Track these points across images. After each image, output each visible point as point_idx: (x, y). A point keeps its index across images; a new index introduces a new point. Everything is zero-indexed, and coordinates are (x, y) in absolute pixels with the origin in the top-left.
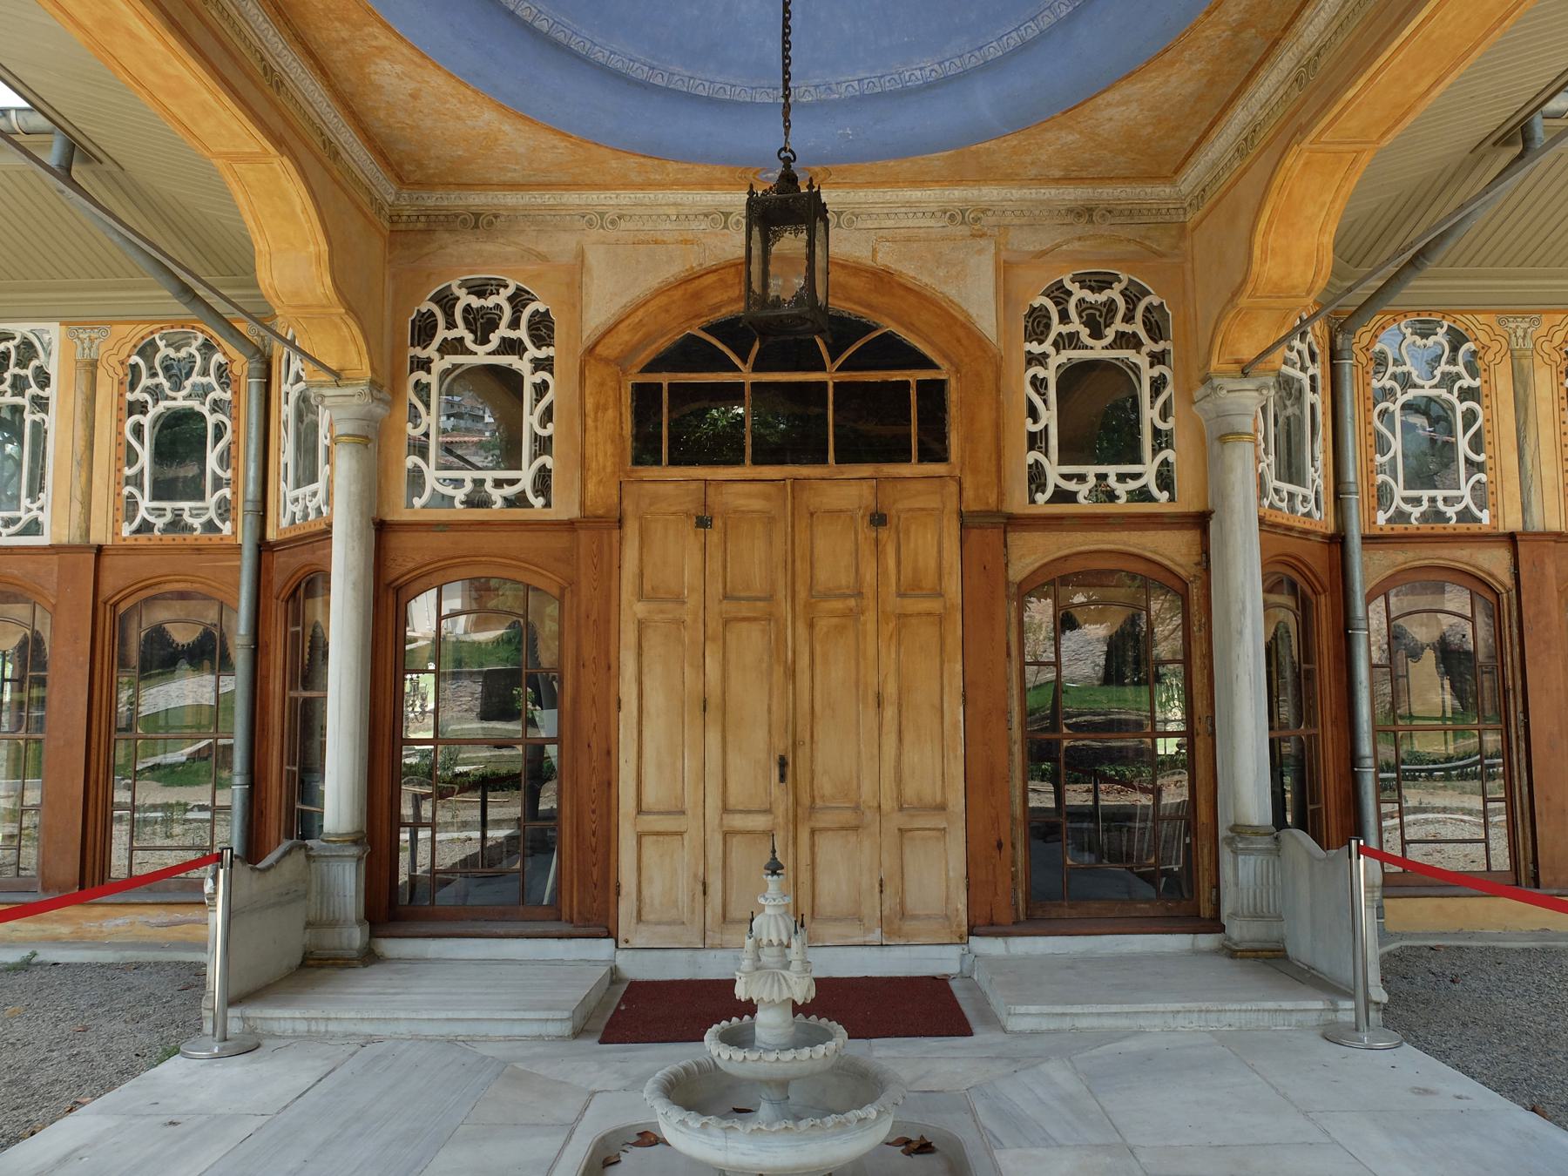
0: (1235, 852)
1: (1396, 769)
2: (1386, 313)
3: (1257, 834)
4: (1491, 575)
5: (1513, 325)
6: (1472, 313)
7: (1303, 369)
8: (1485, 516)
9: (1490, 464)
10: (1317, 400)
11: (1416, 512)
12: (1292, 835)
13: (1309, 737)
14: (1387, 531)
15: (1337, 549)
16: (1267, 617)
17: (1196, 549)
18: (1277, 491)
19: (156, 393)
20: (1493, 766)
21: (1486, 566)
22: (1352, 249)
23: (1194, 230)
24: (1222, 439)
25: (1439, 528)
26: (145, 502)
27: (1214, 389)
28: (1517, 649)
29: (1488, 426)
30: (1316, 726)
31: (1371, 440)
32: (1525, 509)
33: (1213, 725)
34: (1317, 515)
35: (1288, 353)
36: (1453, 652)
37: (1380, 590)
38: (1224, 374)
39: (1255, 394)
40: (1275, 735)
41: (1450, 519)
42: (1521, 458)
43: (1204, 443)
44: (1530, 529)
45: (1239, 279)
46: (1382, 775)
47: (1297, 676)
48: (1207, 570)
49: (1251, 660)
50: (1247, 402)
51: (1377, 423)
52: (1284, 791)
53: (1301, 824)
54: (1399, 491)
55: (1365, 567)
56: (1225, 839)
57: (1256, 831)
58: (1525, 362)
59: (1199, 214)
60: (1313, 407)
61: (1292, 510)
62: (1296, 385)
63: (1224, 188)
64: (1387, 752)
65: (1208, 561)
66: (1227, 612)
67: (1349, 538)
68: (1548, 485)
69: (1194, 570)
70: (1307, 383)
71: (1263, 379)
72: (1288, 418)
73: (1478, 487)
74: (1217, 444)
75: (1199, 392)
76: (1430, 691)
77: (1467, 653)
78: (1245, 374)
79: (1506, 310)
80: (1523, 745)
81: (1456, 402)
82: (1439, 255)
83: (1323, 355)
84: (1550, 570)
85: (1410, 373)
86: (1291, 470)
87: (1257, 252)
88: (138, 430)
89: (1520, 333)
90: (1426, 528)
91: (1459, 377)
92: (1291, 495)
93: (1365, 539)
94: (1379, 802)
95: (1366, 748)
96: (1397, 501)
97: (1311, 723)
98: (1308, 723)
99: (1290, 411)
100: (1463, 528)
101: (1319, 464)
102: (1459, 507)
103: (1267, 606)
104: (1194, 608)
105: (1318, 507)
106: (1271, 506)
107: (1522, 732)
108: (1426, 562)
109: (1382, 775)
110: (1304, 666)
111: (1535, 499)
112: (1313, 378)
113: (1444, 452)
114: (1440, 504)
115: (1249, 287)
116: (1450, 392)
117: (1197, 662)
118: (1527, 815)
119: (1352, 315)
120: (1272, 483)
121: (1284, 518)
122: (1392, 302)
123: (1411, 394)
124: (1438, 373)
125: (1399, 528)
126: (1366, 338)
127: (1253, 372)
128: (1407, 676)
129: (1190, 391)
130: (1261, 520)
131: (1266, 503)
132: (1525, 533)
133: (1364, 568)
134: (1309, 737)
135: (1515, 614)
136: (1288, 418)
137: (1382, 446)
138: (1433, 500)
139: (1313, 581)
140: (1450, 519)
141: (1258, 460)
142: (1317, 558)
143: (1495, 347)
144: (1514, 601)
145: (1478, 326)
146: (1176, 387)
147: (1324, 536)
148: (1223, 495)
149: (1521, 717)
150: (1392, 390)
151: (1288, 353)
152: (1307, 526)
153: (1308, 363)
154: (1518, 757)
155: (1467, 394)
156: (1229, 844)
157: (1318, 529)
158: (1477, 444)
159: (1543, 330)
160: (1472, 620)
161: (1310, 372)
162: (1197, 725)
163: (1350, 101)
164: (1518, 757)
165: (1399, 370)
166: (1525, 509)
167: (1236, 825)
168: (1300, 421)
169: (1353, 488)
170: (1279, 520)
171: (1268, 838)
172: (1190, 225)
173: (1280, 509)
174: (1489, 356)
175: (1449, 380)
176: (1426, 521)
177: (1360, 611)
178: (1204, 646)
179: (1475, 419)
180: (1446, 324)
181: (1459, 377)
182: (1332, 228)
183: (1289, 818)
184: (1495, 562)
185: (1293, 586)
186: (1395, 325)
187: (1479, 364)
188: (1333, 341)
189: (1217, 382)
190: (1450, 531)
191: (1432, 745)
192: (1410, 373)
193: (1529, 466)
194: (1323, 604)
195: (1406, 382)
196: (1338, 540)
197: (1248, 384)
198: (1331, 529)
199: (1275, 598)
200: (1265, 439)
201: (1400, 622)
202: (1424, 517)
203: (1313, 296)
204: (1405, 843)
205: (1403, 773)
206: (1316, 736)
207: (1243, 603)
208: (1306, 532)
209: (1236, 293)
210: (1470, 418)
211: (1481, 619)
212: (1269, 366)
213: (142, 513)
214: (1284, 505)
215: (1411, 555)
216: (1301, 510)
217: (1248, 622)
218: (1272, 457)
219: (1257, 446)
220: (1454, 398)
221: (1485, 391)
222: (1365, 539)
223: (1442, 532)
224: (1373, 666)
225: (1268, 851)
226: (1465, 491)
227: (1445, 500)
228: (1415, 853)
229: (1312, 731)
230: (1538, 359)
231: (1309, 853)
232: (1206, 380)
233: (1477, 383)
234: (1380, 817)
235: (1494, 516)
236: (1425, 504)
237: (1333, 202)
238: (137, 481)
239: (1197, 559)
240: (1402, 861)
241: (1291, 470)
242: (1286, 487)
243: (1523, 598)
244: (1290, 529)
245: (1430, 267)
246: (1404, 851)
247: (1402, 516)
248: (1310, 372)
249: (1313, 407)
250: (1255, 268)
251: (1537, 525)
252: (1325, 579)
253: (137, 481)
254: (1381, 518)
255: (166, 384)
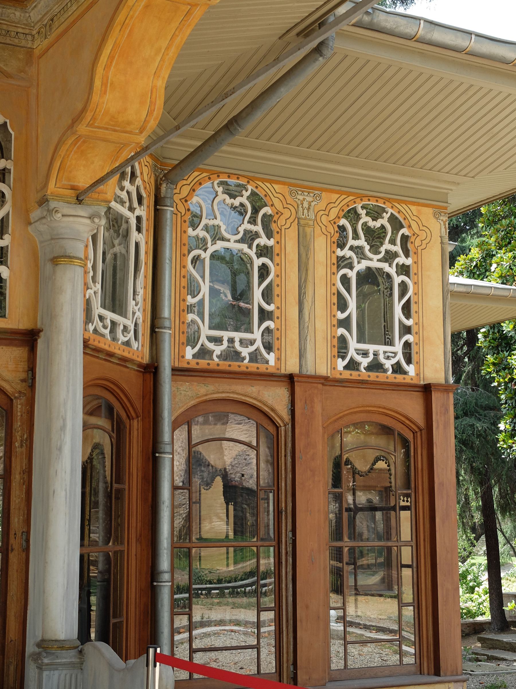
0: (40, 668)
1: (188, 589)
2: (203, 171)
3: (62, 648)
4: (273, 410)
5: (301, 198)
6: (271, 182)
7: (131, 209)
8: (271, 358)
9: (277, 313)
10: (142, 239)
11: (218, 350)
12: (95, 647)
13: (116, 553)
14: (193, 365)
15: (150, 377)
16: (85, 439)
17: (23, 366)
18: (101, 318)
19: (217, 236)
20: (265, 585)
21: (270, 402)
22: (180, 110)
23: (40, 57)
24: (55, 261)
25: (234, 366)
26: (353, 344)
27: (50, 212)
28: (290, 476)
29: (277, 281)
30: (122, 543)
31: (184, 282)
32: (302, 355)
33: (28, 541)
34: (135, 345)
35: (118, 192)
36: (235, 487)
37: (185, 420)
38: (59, 197)
39: (88, 221)
40: (85, 551)
41: (244, 359)
42: (301, 311)
43: (37, 265)
44: (304, 372)
45: (80, 106)
46: (176, 596)
47: (108, 496)
48: (32, 387)
49: (68, 477)
50: (79, 227)
51: (190, 267)
52: (89, 606)
53: (103, 637)
54: (205, 331)
55: (173, 396)
56: (33, 655)
57: (62, 645)
58: (308, 230)
59: (46, 42)
60: (137, 245)
61: (114, 339)
62: (124, 226)
63: (71, 19)
64: (182, 578)
65: (34, 378)
66: (48, 430)
67: (161, 369)
68: (320, 336)
69: (20, 387)
70: (133, 222)
71: (95, 208)
72: (115, 255)
73: (407, 345)
74: (49, 266)
75: (36, 214)
76: (217, 522)
77: (249, 491)
78: (79, 200)
79: (298, 185)
80: (290, 560)
81: (254, 257)
82: (249, 125)
83: (148, 200)
84: (318, 408)
85: (219, 227)
86: (115, 301)
87: (98, 83)
88: (345, 281)
89: (306, 205)
90: (224, 365)
91: (257, 235)
92: (114, 324)
93: (176, 371)
94: (173, 614)
95: (165, 563)
96: (203, 339)
97: (119, 540)
98: (116, 540)
99: (117, 249)
100: (253, 367)
101: (139, 298)
102: (252, 349)
103: (86, 426)
104: (17, 424)
105: (136, 338)
106: (95, 331)
107: (290, 549)
108: (224, 395)
109: (176, 596)
110: (115, 486)
111: (309, 347)
112: (139, 219)
113: (242, 294)
114: (237, 345)
115: (89, 115)
116: (250, 247)
117: (16, 477)
118: (291, 622)
119: (175, 167)
120: (98, 310)
121: (106, 344)
122: (207, 161)
123: (220, 245)
124: (241, 230)
125: (203, 363)
126: (185, 191)
127: (87, 200)
128: (200, 503)
129: (27, 212)
130: (86, 344)
131: (91, 328)
132: (301, 375)
133: (175, 398)
134: (116, 553)
135: (290, 445)
136: (115, 255)
137: (193, 289)
138: (231, 341)
139: (128, 405)
140: (244, 359)
141: (87, 287)
142: (132, 384)
143: (287, 213)
144: (290, 434)
145: (276, 196)
146: (14, 205)
147: (140, 365)
148: (52, 315)
149: (290, 535)
150: (204, 240)
151: (118, 192)
152: (126, 354)
153: (136, 204)
154: (286, 571)
155: (264, 251)
156: (35, 660)
157: (135, 357)
158: (268, 295)
159: (322, 205)
160: (257, 449)
161: (138, 212)
162: (12, 541)
163: (151, 381)
164: (286, 571)
165: (211, 223)
166: (302, 355)
167: (43, 640)
168: (125, 259)
169: (167, 324)
170: (102, 345)
171: (73, 652)
172: (37, 52)
173: (103, 336)
174: (281, 221)
175: (249, 238)
176: (225, 360)
177: (166, 437)
178: (25, 462)
179: (268, 273)
180: (250, 188)
181: (257, 235)
182: (165, 74)
183: (93, 636)
184: (276, 398)
185: (110, 409)
186: (209, 184)
187: (274, 226)
188: (158, 189)
189: (53, 204)
190: (243, 369)
191: (217, 563)
192: (219, 227)
193: (307, 319)
194: (136, 429)
195: (217, 236)
196: (151, 370)
197: (81, 211)
198: (146, 359)
199: (93, 420)
200: (94, 267)
201: (200, 448)
202: (224, 356)
203: (145, 134)
204: (192, 651)
205: (190, 593)
206: (122, 552)
207: (64, 420)
208: (124, 360)
209: (77, 119)
210: (264, 271)
211: (264, 450)
212: (102, 196)
213: (352, 353)
214: (107, 332)
215: (211, 388)
216: (122, 338)
217: (68, 439)
218: (99, 286)
219: (86, 273)
220: (252, 253)
221: (276, 250)
222: (176, 371)
223: (237, 369)
224: (175, 488)
225: (72, 665)
226: (257, 334)
227: (241, 341)
228: (199, 659)
229: (118, 548)
230: (317, 229)
231: (110, 665)
232: (43, 201)
233: (271, 243)
234: (173, 631)
235: (278, 359)
236: (225, 343)
237: (168, 48)
238: (345, 323)
239: (23, 375)
240: (189, 666)
241: (115, 301)
242: (110, 315)
243: (297, 431)
244: (111, 355)
245: (240, 135)
246: (191, 657)
247: (204, 353)
248: (138, 212)
249: (137, 245)
250: (95, 98)
251: (310, 369)
252: (138, 405)
253: (345, 323)
254: (189, 352)
255: (367, 247)
